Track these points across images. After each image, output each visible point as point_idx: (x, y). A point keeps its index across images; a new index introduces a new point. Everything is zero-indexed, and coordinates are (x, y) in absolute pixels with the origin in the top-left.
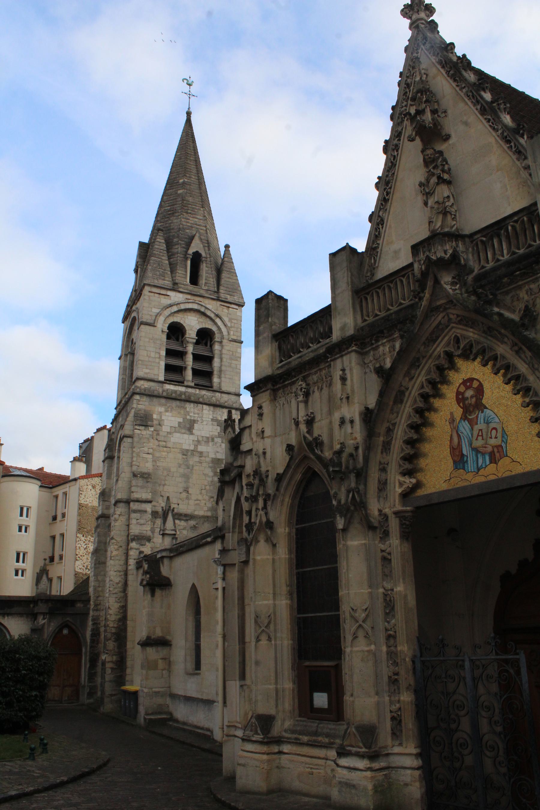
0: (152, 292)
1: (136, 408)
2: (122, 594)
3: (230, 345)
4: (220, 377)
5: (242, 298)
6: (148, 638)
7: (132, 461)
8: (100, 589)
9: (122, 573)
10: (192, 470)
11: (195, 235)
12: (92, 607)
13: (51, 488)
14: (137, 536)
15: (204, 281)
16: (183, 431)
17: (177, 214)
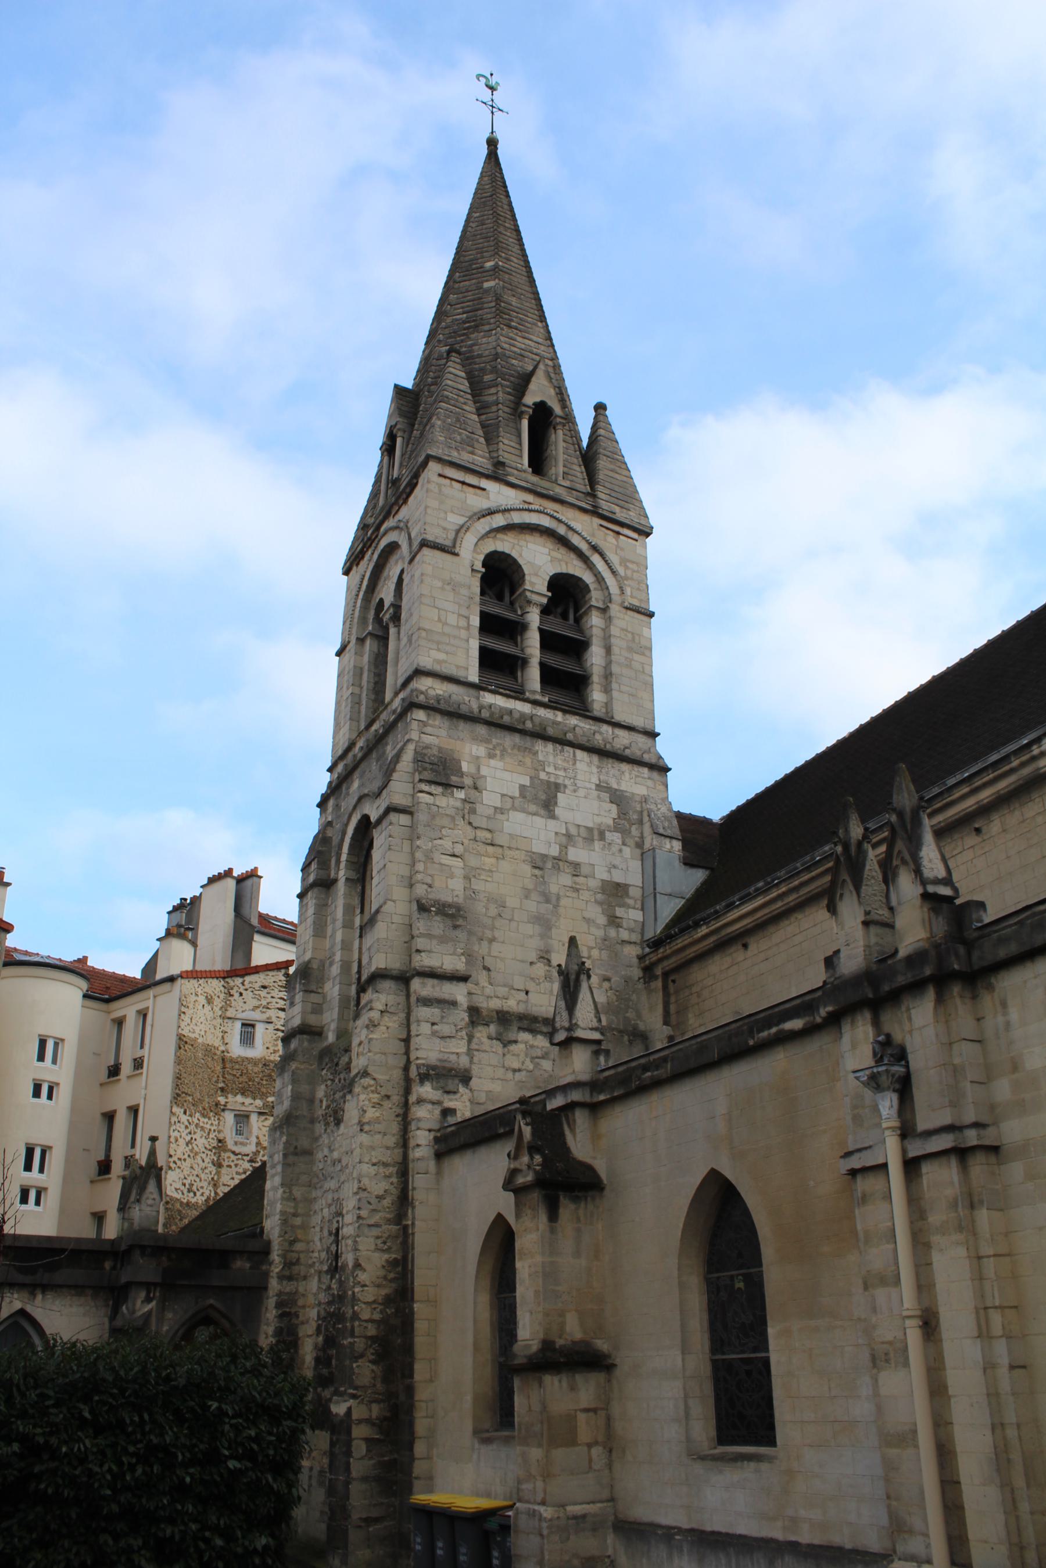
0: (445, 477)
1: (417, 742)
2: (394, 1228)
3: (627, 618)
4: (607, 690)
5: (647, 517)
6: (547, 1345)
7: (414, 872)
8: (298, 1221)
9: (392, 1170)
10: (556, 906)
11: (532, 373)
12: (276, 1269)
13: (107, 1001)
14: (434, 1068)
15: (561, 469)
16: (533, 808)
17: (486, 328)
